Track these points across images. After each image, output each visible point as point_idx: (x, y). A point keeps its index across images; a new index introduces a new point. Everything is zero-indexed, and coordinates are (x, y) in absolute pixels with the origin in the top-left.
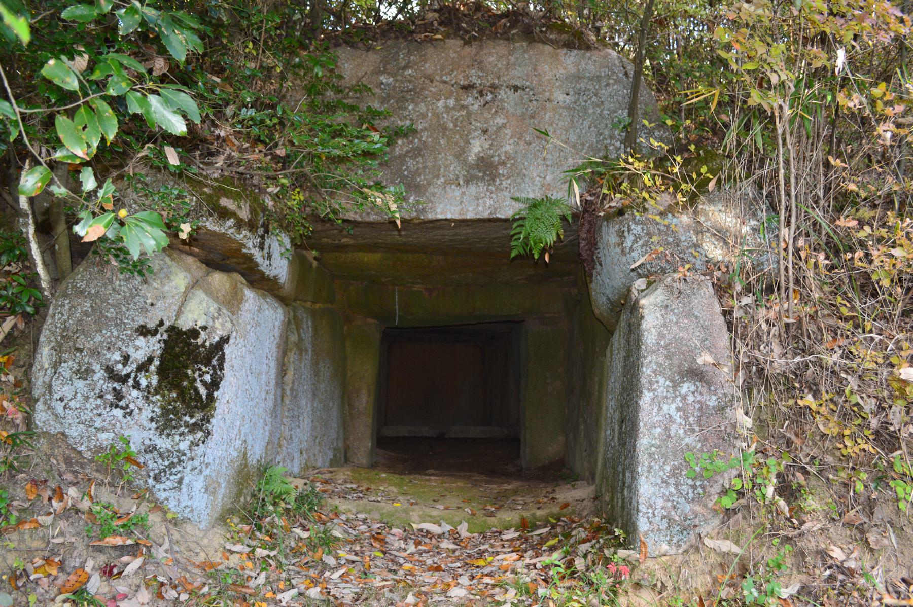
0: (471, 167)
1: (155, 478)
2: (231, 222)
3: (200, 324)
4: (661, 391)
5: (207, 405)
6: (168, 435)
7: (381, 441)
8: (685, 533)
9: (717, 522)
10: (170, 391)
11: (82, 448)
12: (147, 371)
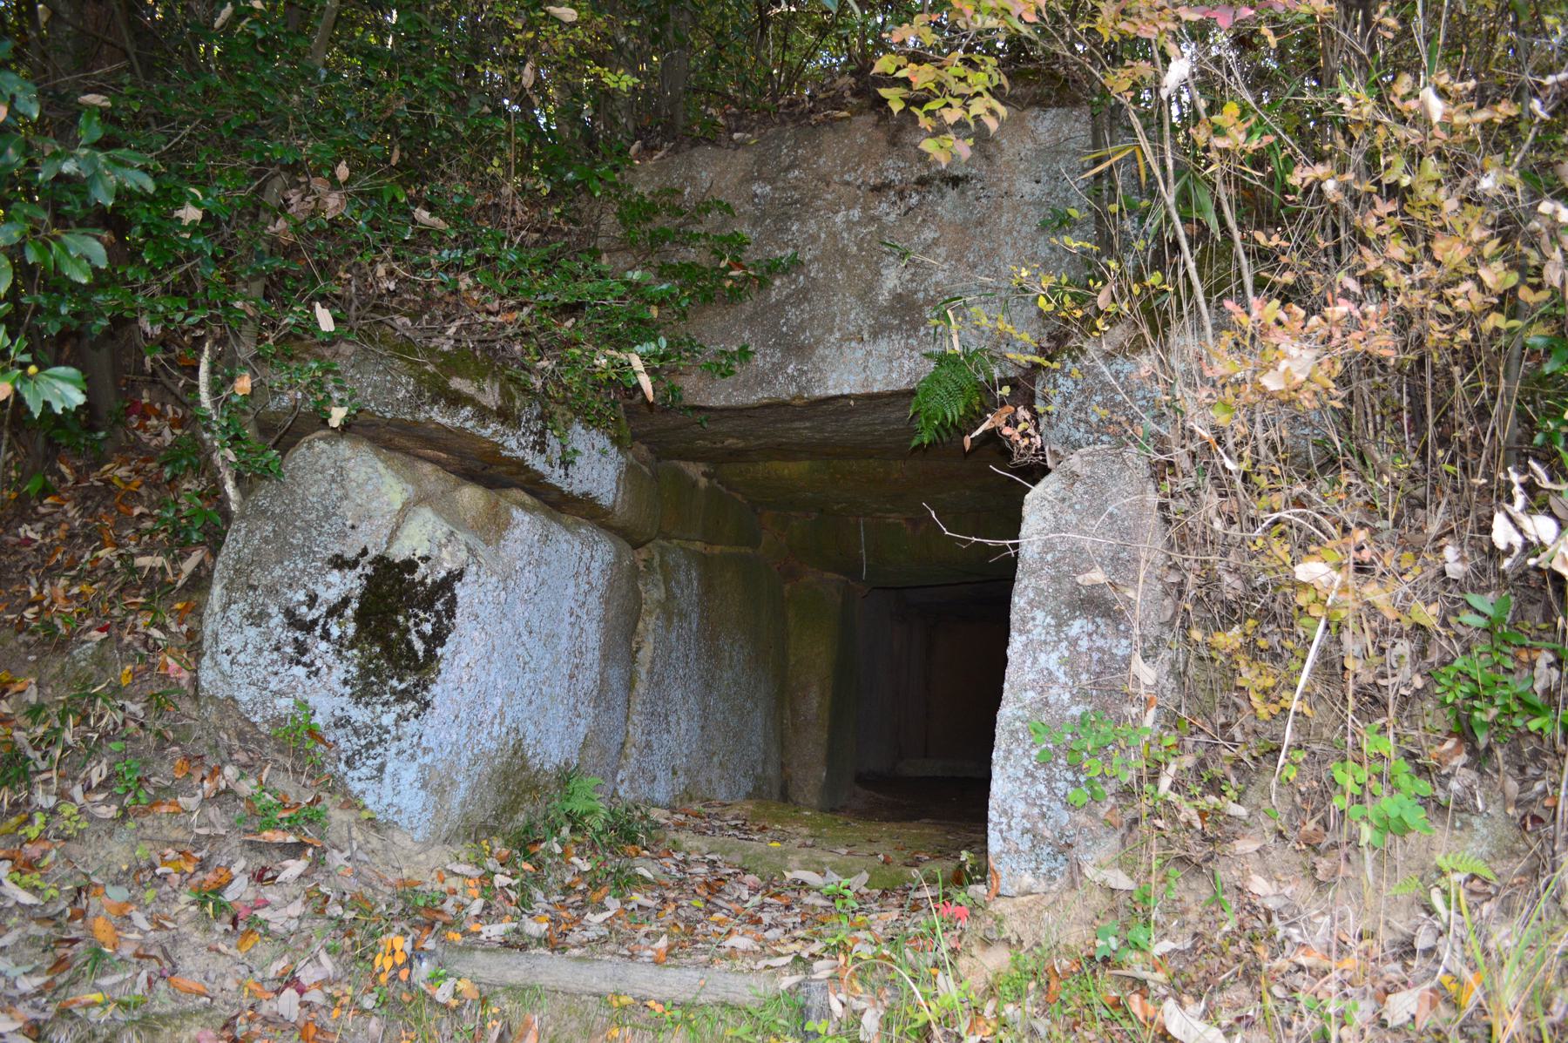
0: (882, 311)
1: (347, 762)
2: (467, 411)
3: (419, 553)
4: (1038, 633)
5: (425, 666)
6: (367, 704)
8: (1060, 858)
9: (1114, 841)
10: (371, 645)
11: (257, 719)
12: (341, 616)
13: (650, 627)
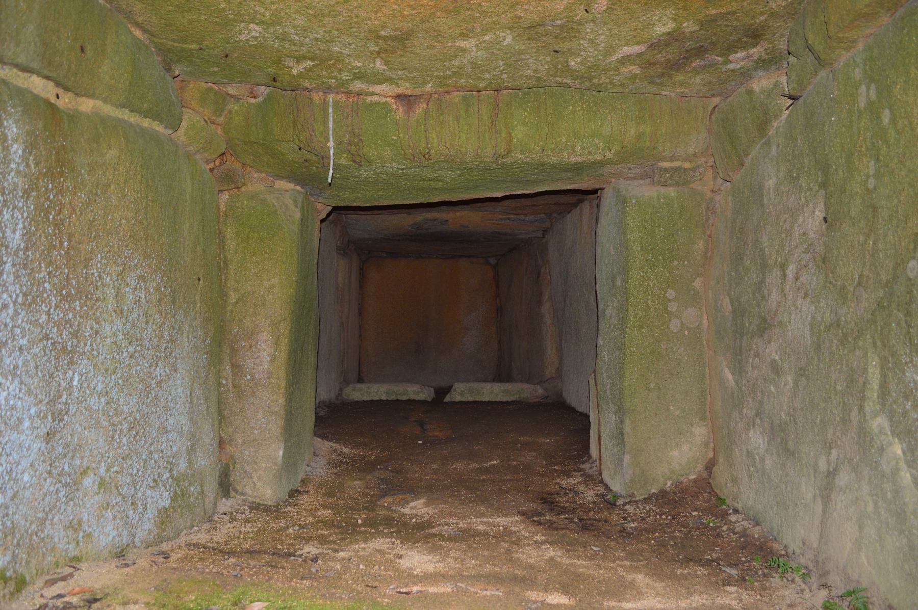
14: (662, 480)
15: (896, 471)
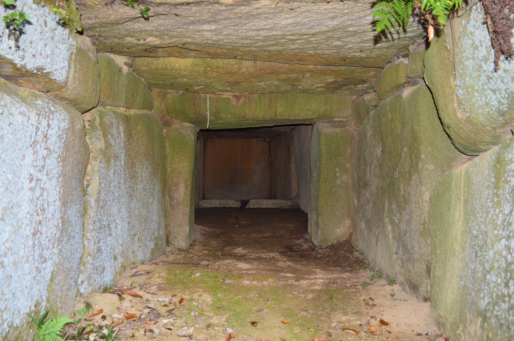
7: (201, 215)
13: (96, 169)
14: (333, 240)
15: (389, 234)
